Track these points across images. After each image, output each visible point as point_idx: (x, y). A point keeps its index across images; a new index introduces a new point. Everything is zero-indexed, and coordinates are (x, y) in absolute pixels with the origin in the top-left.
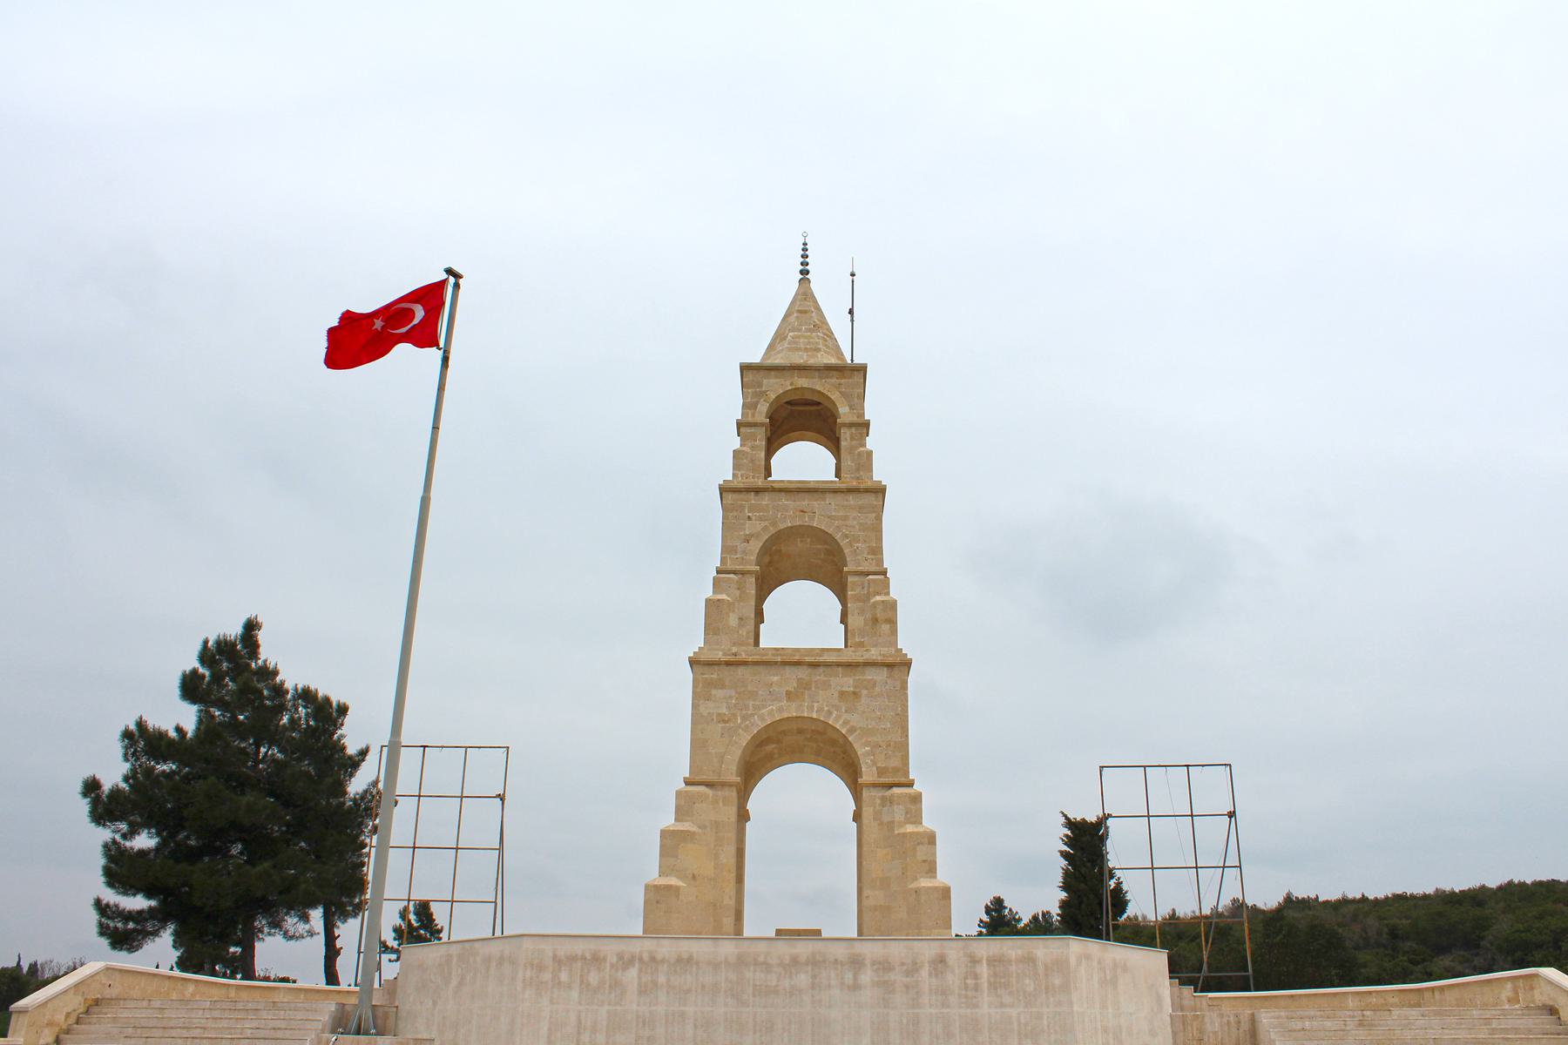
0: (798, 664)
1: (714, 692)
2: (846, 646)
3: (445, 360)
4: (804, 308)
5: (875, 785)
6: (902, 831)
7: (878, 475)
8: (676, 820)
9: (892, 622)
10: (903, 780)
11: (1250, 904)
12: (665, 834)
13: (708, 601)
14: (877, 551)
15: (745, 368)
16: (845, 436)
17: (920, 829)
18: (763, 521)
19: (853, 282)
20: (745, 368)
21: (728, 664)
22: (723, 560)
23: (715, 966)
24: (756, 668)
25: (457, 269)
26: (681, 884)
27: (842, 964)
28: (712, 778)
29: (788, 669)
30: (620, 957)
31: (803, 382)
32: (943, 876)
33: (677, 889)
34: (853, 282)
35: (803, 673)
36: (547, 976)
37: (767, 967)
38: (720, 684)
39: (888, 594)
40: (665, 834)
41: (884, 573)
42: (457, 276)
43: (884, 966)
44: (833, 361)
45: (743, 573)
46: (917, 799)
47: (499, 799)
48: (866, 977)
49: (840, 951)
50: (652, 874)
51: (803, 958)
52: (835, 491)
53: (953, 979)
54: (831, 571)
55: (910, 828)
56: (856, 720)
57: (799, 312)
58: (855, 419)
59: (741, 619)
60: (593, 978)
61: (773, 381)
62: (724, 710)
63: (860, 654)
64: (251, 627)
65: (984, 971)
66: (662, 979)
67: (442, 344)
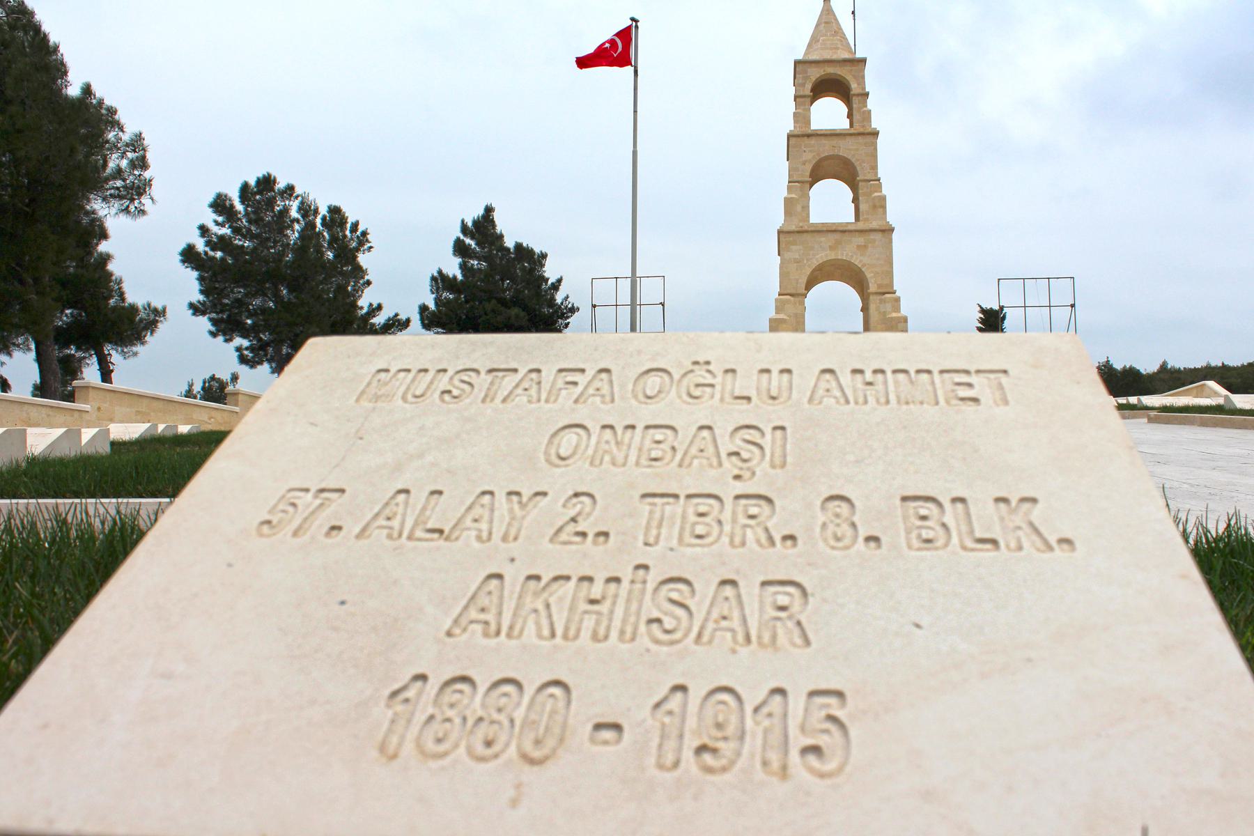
0: (835, 231)
9: (884, 207)
10: (891, 291)
14: (874, 168)
15: (797, 63)
16: (855, 101)
17: (899, 315)
18: (809, 156)
20: (797, 63)
21: (798, 232)
25: (637, 17)
28: (793, 291)
31: (830, 70)
35: (837, 236)
38: (794, 243)
39: (881, 192)
40: (771, 320)
41: (879, 180)
42: (636, 21)
44: (846, 56)
46: (898, 300)
54: (848, 172)
55: (894, 315)
56: (866, 260)
57: (826, 23)
62: (797, 257)
64: (489, 210)
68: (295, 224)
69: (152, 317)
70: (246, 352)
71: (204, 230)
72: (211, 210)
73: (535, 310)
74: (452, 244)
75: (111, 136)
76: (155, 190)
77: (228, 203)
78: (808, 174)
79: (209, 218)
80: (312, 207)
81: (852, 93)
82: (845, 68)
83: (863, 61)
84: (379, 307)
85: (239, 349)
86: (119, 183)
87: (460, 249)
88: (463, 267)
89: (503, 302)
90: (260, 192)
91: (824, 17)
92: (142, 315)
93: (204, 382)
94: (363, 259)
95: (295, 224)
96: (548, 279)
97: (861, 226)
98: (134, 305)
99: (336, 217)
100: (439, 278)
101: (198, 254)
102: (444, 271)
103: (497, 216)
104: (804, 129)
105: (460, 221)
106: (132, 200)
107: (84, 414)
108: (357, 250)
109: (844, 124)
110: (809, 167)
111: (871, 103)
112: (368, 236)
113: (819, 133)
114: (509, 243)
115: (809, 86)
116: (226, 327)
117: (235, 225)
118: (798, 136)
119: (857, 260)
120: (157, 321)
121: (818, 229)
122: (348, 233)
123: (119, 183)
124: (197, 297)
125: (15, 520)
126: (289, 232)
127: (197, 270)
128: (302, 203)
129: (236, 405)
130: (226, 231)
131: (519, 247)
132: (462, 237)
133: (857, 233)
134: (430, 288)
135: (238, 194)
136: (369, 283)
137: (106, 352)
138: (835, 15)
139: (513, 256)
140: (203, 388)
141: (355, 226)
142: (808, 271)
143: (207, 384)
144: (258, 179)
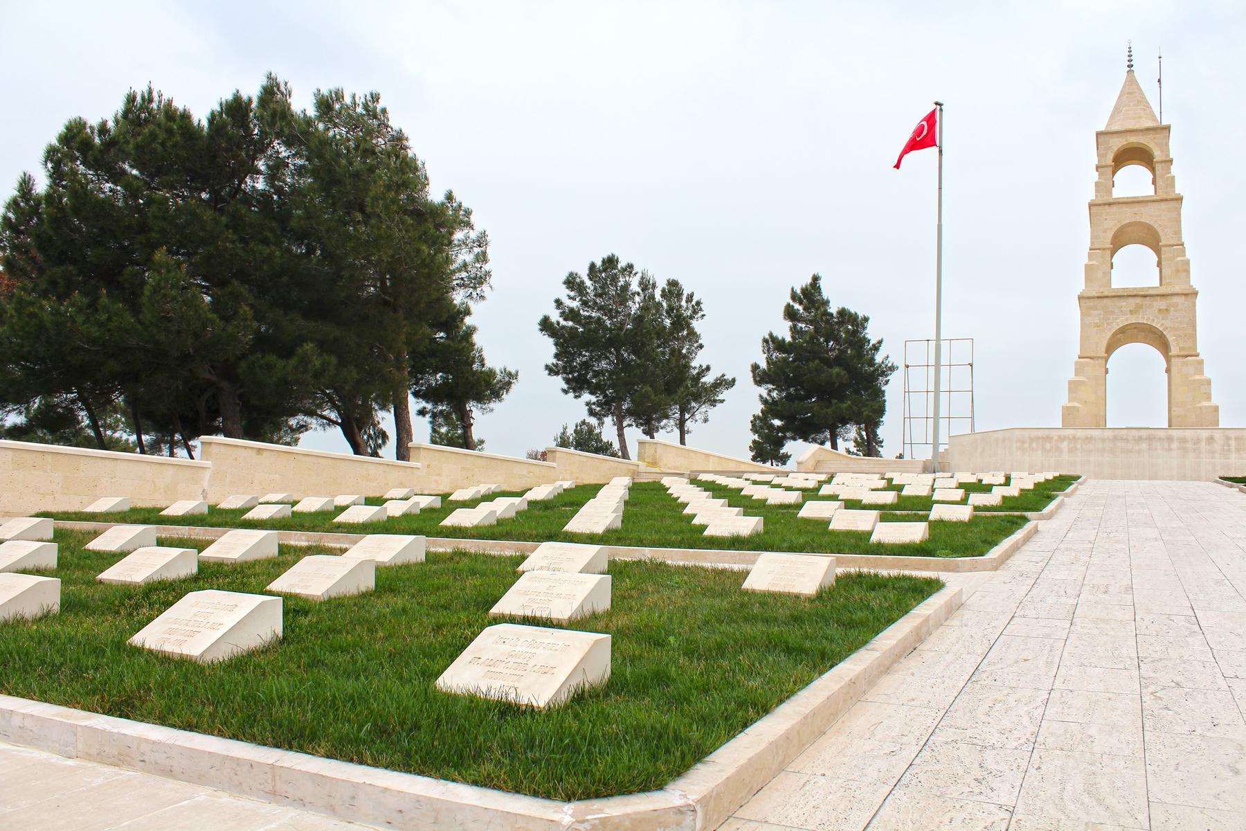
1: (1092, 312)
2: (1161, 284)
3: (941, 151)
4: (1131, 87)
5: (1178, 356)
6: (1192, 378)
7: (1179, 190)
8: (1075, 375)
9: (1187, 271)
10: (1194, 353)
11: (148, 647)
12: (1070, 382)
13: (1086, 265)
14: (1178, 232)
15: (1099, 134)
16: (1158, 167)
17: (1203, 378)
18: (1114, 220)
19: (1160, 62)
20: (1099, 134)
21: (1098, 297)
22: (1092, 243)
23: (1103, 440)
24: (1114, 299)
25: (941, 102)
26: (1079, 405)
27: (1163, 439)
28: (1092, 354)
29: (1130, 300)
30: (1060, 437)
31: (1133, 139)
32: (1215, 400)
33: (1078, 408)
34: (1160, 62)
35: (1138, 300)
36: (1027, 445)
37: (1127, 440)
38: (1095, 308)
39: (1185, 256)
40: (1070, 382)
41: (1183, 245)
42: (940, 105)
43: (1183, 440)
44: (1150, 124)
45: (1104, 249)
46: (1201, 362)
47: (969, 366)
48: (1175, 445)
49: (1162, 434)
50: (1065, 401)
51: (1144, 437)
52: (1154, 201)
53: (1217, 446)
54: (1151, 239)
55: (1197, 377)
56: (1167, 323)
57: (1129, 93)
58: (1164, 158)
59: (1104, 273)
60: (1048, 446)
61: (1116, 139)
62: (1097, 321)
63: (1169, 289)
64: (816, 279)
65: (1233, 443)
66: (1079, 446)
67: (938, 144)
68: (636, 296)
69: (507, 379)
70: (593, 407)
71: (559, 303)
72: (565, 286)
73: (856, 369)
74: (783, 309)
75: (458, 235)
76: (492, 280)
77: (578, 280)
78: (1109, 240)
79: (563, 293)
80: (651, 282)
81: (1155, 160)
82: (1148, 136)
83: (1168, 128)
84: (708, 368)
85: (588, 404)
86: (464, 275)
87: (790, 314)
88: (794, 330)
89: (827, 362)
90: (605, 270)
91: (1127, 87)
92: (499, 377)
93: (577, 426)
94: (696, 325)
95: (636, 296)
96: (869, 341)
97: (1163, 290)
98: (493, 369)
99: (673, 290)
100: (770, 340)
101: (552, 324)
102: (775, 334)
103: (822, 284)
104: (1105, 198)
105: (790, 289)
106: (475, 288)
107: (415, 470)
108: (691, 317)
109: (1148, 190)
110: (1110, 235)
111: (1174, 170)
112: (701, 305)
113: (1120, 201)
114: (833, 309)
115: (1111, 156)
116: (577, 385)
117: (584, 298)
118: (1099, 205)
119: (1157, 325)
120: (511, 383)
121: (1118, 294)
122: (683, 303)
123: (464, 275)
124: (551, 360)
125: (866, 464)
126: (630, 303)
127: (552, 337)
128: (642, 278)
129: (554, 461)
130: (575, 304)
131: (842, 312)
132: (792, 303)
133: (1159, 298)
134: (762, 348)
135: (587, 272)
136: (701, 346)
137: (468, 409)
138: (1138, 85)
139: (836, 320)
140: (576, 431)
141: (690, 298)
142: (1109, 334)
143: (579, 428)
144: (604, 259)
